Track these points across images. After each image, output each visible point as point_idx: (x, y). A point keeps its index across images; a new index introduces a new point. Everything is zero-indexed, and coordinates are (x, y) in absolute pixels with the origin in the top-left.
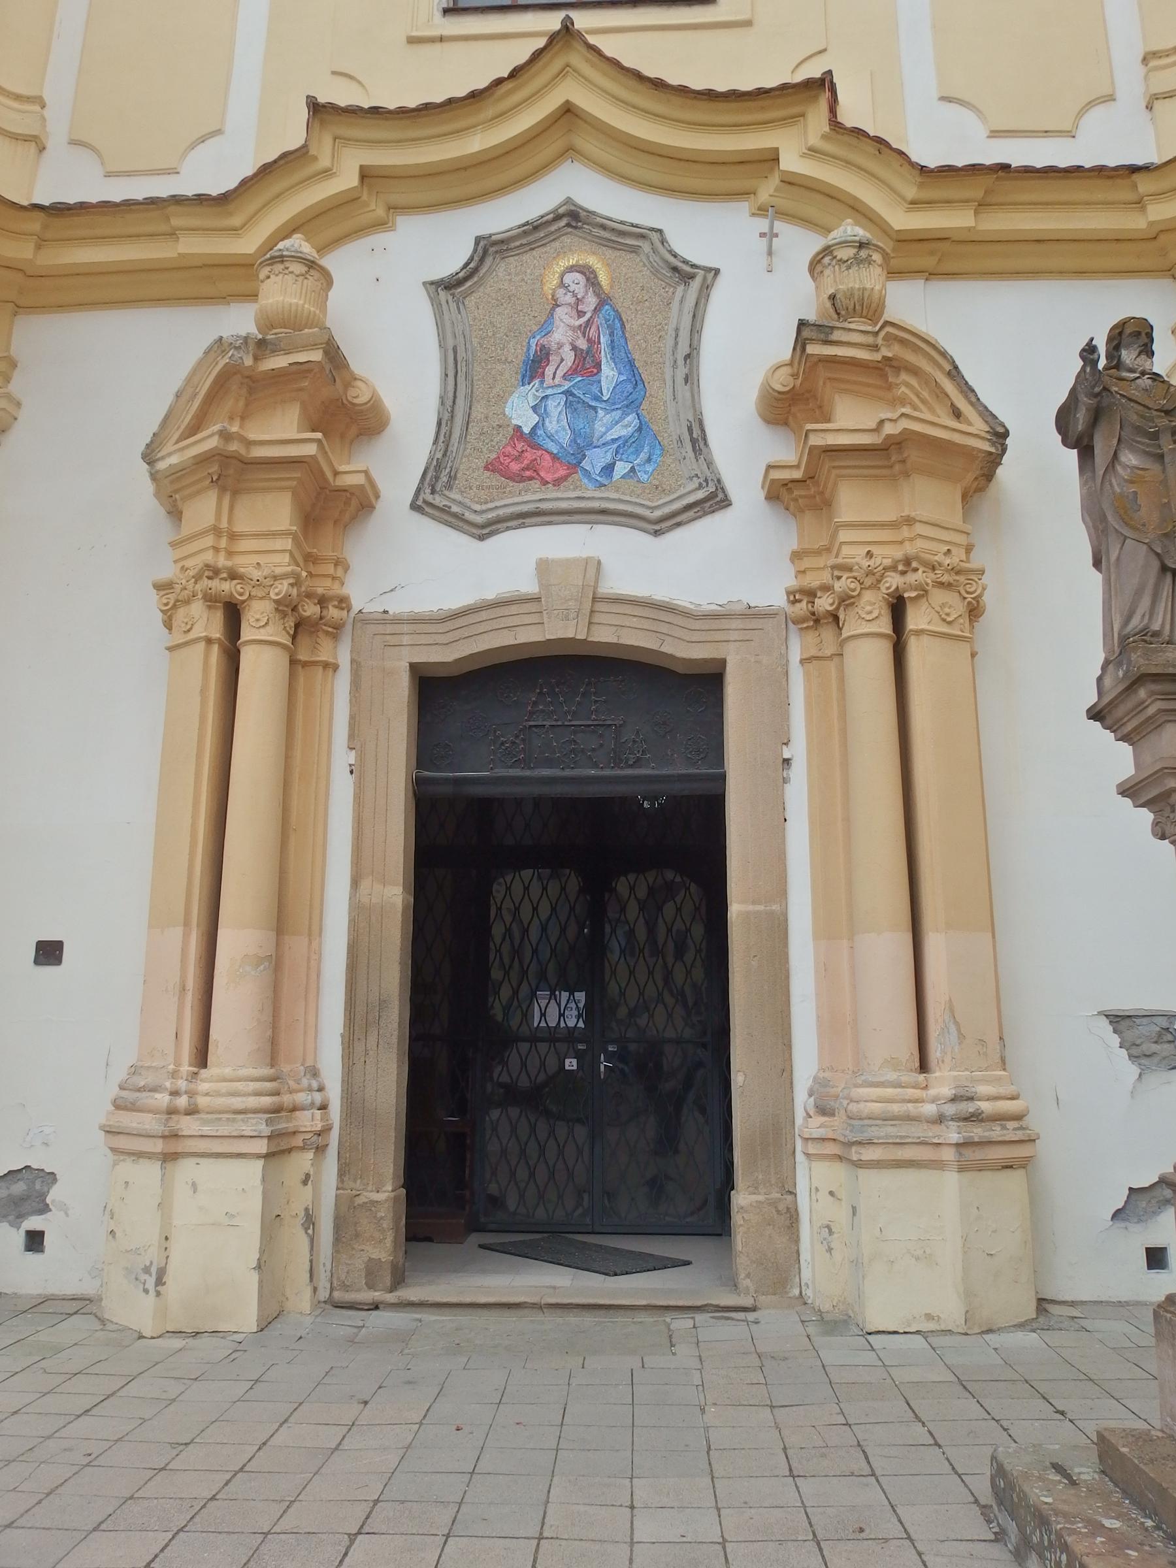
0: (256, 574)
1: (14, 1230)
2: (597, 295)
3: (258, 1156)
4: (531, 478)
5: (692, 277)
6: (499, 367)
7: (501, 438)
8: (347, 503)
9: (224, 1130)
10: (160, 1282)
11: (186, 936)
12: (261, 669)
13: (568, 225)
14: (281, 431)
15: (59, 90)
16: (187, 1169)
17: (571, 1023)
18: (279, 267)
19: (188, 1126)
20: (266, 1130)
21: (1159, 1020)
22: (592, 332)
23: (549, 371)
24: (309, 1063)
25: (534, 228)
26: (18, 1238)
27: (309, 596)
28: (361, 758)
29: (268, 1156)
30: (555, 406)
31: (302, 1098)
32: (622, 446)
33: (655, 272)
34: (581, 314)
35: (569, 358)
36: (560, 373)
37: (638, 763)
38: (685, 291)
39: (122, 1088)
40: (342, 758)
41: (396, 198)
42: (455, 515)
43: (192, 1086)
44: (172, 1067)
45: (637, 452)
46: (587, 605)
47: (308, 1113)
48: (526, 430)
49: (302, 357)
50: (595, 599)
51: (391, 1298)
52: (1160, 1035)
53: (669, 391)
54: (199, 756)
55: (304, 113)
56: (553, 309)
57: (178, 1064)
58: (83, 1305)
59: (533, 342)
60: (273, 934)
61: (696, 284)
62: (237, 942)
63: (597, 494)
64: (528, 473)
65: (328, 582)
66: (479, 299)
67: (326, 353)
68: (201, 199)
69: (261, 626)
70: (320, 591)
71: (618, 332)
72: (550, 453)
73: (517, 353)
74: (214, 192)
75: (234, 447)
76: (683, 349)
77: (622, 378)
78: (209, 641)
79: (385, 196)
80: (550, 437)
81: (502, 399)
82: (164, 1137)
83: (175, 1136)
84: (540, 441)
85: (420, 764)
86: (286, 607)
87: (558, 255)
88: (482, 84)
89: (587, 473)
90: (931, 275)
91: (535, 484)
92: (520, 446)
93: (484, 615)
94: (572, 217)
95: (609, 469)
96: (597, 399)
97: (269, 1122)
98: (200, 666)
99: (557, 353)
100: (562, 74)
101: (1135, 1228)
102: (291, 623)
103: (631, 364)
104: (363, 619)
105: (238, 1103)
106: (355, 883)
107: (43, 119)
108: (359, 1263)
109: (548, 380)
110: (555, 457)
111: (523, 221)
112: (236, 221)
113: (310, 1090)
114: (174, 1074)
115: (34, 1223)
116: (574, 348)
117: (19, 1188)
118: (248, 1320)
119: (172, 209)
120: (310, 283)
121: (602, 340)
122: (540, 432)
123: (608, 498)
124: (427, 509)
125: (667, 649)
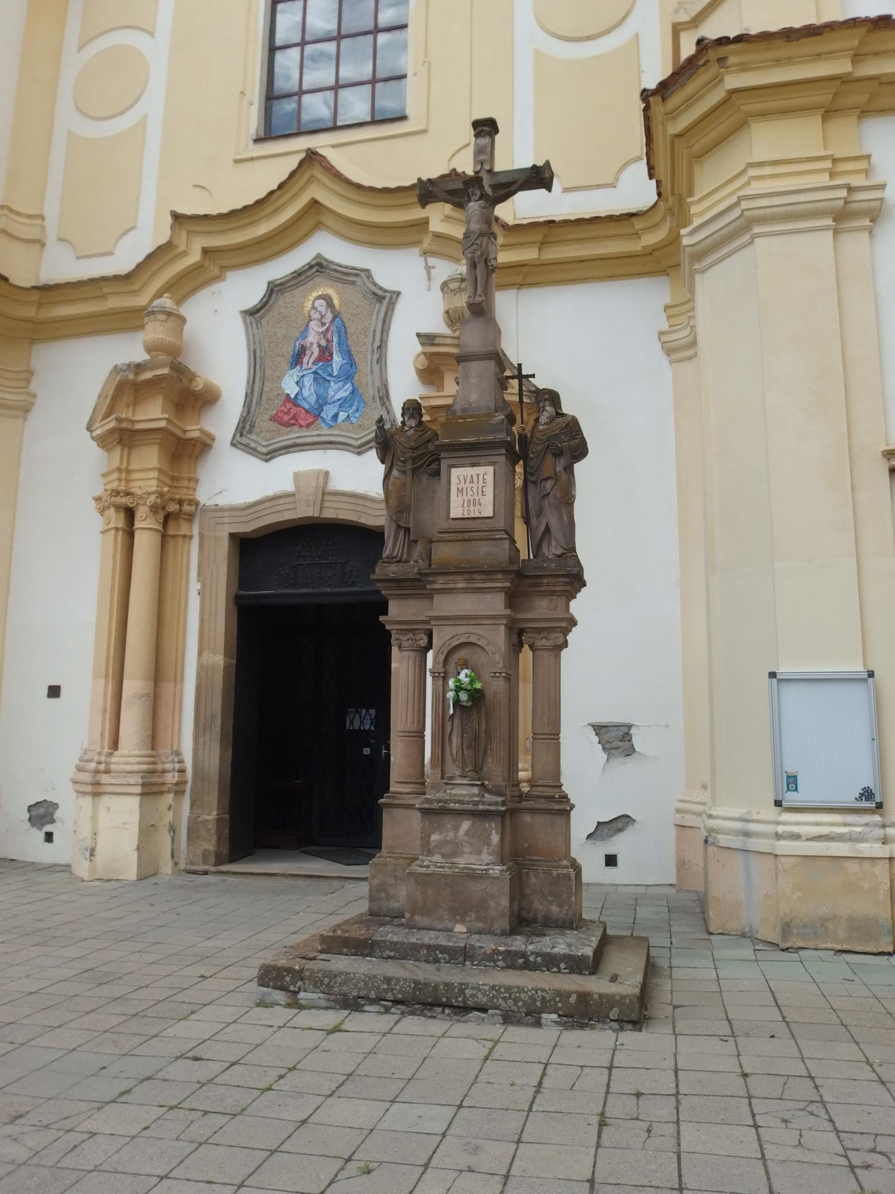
0: (139, 492)
1: (39, 832)
2: (332, 312)
3: (137, 794)
4: (294, 424)
5: (384, 298)
6: (279, 359)
7: (279, 402)
8: (194, 445)
9: (121, 781)
10: (92, 854)
11: (106, 684)
12: (145, 543)
13: (317, 271)
14: (153, 413)
15: (52, 209)
16: (105, 801)
17: (367, 727)
18: (152, 317)
19: (105, 779)
20: (140, 781)
21: (622, 728)
22: (329, 335)
23: (305, 360)
24: (175, 748)
25: (298, 274)
26: (41, 836)
27: (172, 500)
28: (203, 586)
29: (142, 794)
30: (308, 381)
31: (169, 766)
32: (344, 403)
33: (364, 297)
34: (323, 324)
35: (316, 351)
36: (311, 361)
37: (353, 584)
38: (380, 307)
39: (80, 760)
40: (195, 586)
41: (225, 262)
42: (252, 448)
43: (108, 759)
44: (99, 750)
45: (351, 406)
46: (319, 498)
47: (171, 774)
48: (292, 396)
49: (159, 372)
50: (324, 494)
51: (213, 869)
52: (623, 737)
53: (369, 368)
54: (112, 591)
55: (169, 220)
56: (308, 323)
57: (102, 748)
58: (67, 868)
59: (297, 343)
60: (152, 683)
61: (385, 302)
62: (133, 686)
63: (328, 432)
64: (292, 422)
65: (185, 491)
66: (268, 319)
67: (172, 368)
68: (116, 278)
69: (145, 522)
70: (177, 497)
71: (343, 334)
72: (305, 409)
73: (288, 351)
74: (123, 273)
75: (124, 425)
76: (377, 343)
77: (345, 362)
78: (117, 529)
79: (217, 263)
80: (305, 399)
81: (280, 378)
82: (92, 784)
83: (98, 784)
84: (299, 402)
85: (241, 586)
86: (154, 509)
87: (311, 291)
88: (262, 194)
89: (323, 420)
90: (520, 286)
91: (296, 428)
92: (289, 405)
93: (267, 505)
94: (319, 267)
95: (336, 416)
96: (330, 375)
97: (142, 777)
98: (113, 543)
99: (310, 349)
100: (310, 181)
101: (599, 844)
102: (161, 517)
103: (349, 352)
104: (206, 510)
105: (129, 768)
106: (200, 654)
107: (43, 228)
108: (199, 851)
109: (305, 366)
110: (307, 411)
111: (293, 270)
112: (136, 287)
113: (173, 762)
114: (100, 754)
115: (48, 828)
116: (319, 346)
117: (42, 811)
118: (131, 873)
119: (103, 283)
120: (169, 324)
121: (334, 339)
122: (299, 397)
123: (334, 434)
124: (239, 445)
125: (362, 520)
